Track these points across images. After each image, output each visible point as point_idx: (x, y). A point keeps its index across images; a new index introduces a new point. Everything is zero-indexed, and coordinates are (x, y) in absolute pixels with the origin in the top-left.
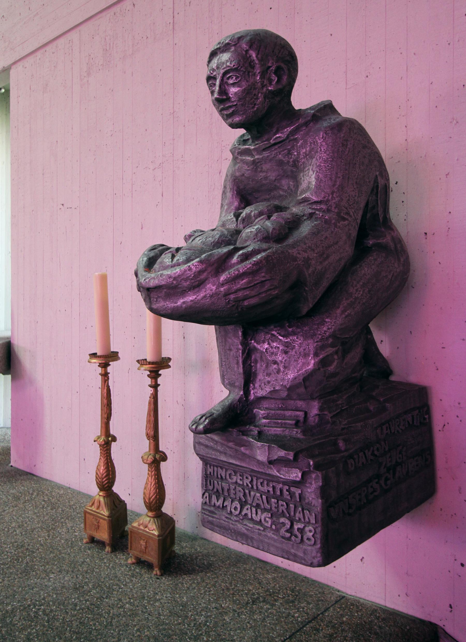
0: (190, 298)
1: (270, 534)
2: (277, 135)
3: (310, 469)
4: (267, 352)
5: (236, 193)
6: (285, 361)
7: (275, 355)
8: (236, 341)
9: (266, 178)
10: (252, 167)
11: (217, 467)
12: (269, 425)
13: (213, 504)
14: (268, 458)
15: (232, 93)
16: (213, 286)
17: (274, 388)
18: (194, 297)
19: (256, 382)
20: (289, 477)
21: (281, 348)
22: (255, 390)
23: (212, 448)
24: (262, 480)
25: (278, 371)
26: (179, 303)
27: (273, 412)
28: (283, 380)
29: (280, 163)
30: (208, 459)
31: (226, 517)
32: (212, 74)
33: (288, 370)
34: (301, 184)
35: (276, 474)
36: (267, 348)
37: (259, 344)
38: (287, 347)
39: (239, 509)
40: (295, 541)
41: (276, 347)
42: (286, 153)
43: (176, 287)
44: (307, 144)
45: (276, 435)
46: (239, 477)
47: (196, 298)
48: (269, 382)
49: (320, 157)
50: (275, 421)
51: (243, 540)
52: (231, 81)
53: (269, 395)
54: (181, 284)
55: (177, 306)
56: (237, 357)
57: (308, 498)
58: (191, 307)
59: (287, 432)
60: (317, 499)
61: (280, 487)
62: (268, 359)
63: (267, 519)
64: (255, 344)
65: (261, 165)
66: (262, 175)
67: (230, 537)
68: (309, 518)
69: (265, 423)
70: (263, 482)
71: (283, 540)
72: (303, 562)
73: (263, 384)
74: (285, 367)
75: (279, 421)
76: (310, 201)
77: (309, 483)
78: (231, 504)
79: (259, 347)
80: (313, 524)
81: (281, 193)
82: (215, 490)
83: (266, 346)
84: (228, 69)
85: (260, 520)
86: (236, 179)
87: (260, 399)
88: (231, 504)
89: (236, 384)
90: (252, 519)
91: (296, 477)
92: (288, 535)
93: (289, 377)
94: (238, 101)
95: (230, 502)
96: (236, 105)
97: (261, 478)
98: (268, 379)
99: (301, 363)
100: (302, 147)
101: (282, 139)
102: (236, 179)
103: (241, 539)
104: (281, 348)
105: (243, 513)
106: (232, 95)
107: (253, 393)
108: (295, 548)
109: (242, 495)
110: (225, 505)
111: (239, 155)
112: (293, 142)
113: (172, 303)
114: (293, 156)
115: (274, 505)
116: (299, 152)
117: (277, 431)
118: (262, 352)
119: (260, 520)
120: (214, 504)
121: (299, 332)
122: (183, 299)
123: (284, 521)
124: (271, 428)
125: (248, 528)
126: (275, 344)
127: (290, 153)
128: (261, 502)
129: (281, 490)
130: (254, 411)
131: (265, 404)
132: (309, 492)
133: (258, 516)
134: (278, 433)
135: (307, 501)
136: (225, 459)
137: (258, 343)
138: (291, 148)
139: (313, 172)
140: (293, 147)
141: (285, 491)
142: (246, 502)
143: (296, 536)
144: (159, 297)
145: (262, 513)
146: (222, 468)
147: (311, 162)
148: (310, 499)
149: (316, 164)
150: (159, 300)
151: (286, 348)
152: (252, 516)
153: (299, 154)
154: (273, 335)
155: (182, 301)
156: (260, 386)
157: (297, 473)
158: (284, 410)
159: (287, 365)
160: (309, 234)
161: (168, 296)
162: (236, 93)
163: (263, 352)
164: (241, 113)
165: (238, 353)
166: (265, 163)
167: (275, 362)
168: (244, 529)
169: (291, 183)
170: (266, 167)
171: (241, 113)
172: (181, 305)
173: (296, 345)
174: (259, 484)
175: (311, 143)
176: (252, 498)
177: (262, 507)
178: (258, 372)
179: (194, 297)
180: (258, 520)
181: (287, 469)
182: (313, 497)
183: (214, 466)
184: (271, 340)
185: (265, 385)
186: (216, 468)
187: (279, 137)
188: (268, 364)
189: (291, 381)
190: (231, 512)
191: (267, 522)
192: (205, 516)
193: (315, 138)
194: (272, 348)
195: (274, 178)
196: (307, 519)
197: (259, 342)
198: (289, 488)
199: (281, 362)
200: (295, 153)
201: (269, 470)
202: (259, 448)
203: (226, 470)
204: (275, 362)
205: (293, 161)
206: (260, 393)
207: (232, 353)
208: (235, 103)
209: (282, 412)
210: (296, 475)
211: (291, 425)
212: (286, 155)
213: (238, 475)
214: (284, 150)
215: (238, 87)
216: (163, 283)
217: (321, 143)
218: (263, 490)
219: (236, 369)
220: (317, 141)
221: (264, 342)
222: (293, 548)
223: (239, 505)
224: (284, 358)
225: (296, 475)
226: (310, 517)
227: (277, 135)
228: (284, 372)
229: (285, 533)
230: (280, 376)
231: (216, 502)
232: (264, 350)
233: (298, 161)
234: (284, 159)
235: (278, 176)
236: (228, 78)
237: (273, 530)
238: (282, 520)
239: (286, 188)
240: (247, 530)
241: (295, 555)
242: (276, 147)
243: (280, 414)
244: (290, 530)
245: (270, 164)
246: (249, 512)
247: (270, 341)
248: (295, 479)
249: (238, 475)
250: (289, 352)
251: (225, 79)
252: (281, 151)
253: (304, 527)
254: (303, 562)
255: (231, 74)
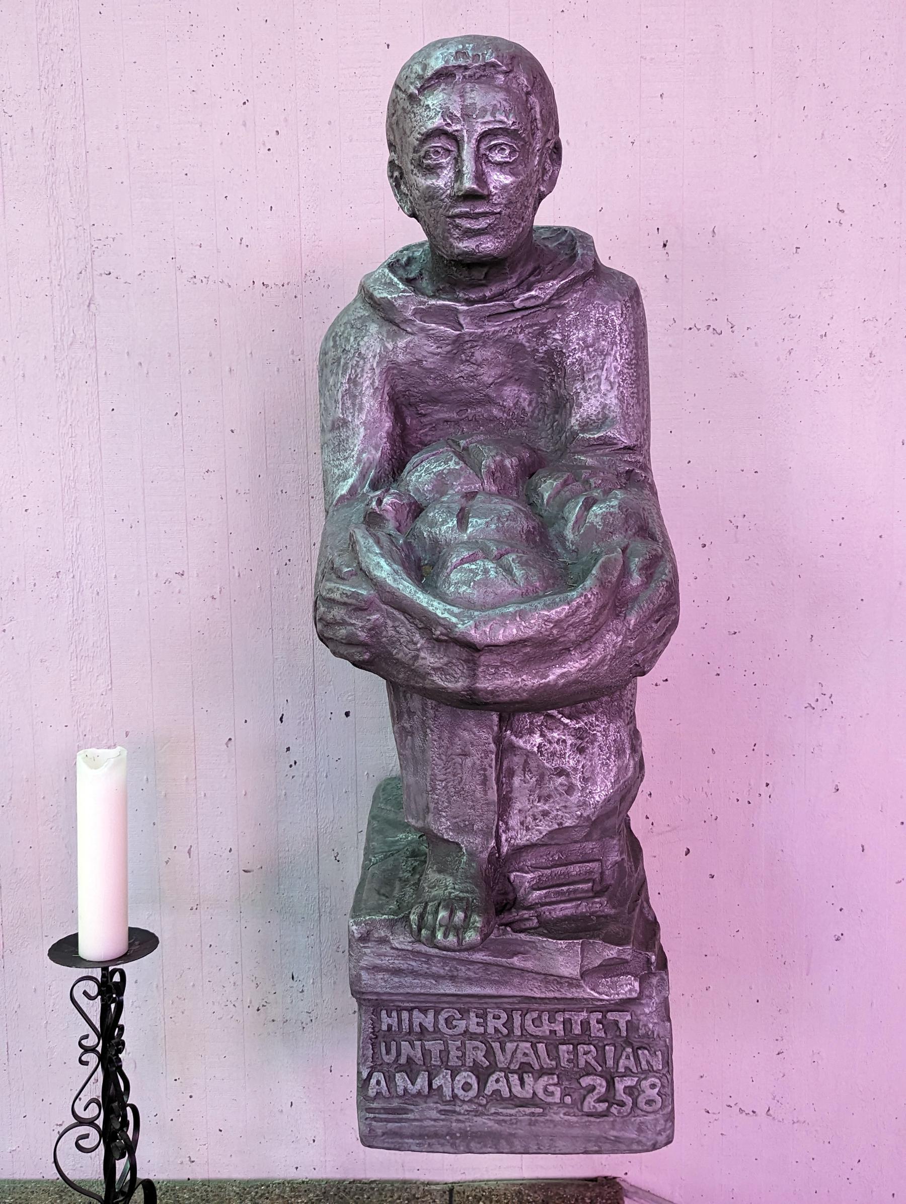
0: (574, 665)
1: (560, 1116)
2: (533, 293)
3: (649, 968)
4: (541, 752)
5: (387, 399)
6: (583, 767)
7: (560, 758)
8: (484, 735)
9: (473, 377)
10: (449, 348)
11: (410, 1010)
12: (548, 900)
13: (401, 1092)
14: (582, 967)
15: (497, 184)
16: (618, 635)
17: (560, 824)
18: (584, 662)
19: (509, 817)
20: (618, 994)
21: (569, 742)
22: (512, 833)
23: (414, 973)
24: (535, 1015)
25: (570, 789)
26: (552, 677)
27: (549, 871)
28: (583, 804)
29: (516, 350)
30: (384, 998)
31: (440, 1112)
32: (448, 125)
33: (592, 785)
34: (580, 406)
35: (590, 994)
36: (540, 744)
37: (521, 737)
38: (581, 738)
39: (475, 1086)
40: (619, 1112)
41: (559, 740)
42: (537, 332)
43: (554, 642)
44: (589, 321)
45: (566, 918)
46: (475, 1020)
47: (588, 664)
48: (545, 814)
49: (621, 355)
50: (557, 889)
51: (485, 1146)
52: (498, 157)
53: (546, 840)
54: (565, 636)
55: (547, 685)
56: (485, 770)
57: (645, 1025)
58: (576, 682)
59: (583, 908)
60: (662, 1023)
61: (582, 1018)
62: (544, 767)
63: (551, 1088)
64: (513, 738)
65: (472, 347)
66: (468, 369)
67: (451, 1150)
68: (648, 1062)
69: (540, 897)
70: (540, 1017)
71: (592, 1119)
72: (635, 1147)
73: (529, 819)
74: (585, 780)
75: (565, 888)
76: (616, 444)
77: (647, 996)
78: (453, 1080)
79: (521, 743)
80: (658, 1071)
81: (495, 412)
82: (403, 1060)
83: (537, 739)
84: (498, 126)
85: (534, 1093)
86: (393, 368)
87: (519, 851)
88: (453, 1080)
89: (475, 827)
90: (512, 1097)
91: (630, 990)
92: (603, 1106)
93: (597, 798)
94: (505, 205)
95: (449, 1076)
96: (500, 213)
97: (535, 1010)
98: (542, 806)
99: (615, 769)
100: (575, 323)
101: (540, 301)
102: (393, 368)
103: (479, 1146)
104: (569, 742)
105: (488, 1091)
106: (495, 188)
107: (506, 840)
108: (618, 1126)
109: (480, 1055)
110: (435, 1087)
111: (418, 316)
112: (555, 311)
113: (534, 678)
114: (549, 341)
115: (566, 1055)
116: (569, 336)
117: (567, 908)
118: (528, 754)
119: (534, 1093)
120: (405, 1090)
121: (596, 708)
122: (560, 667)
123: (592, 1083)
124: (555, 906)
125: (502, 1118)
126: (555, 735)
127: (542, 333)
128: (532, 1059)
129: (585, 1024)
130: (512, 877)
131: (529, 860)
132: (646, 1015)
133: (527, 1087)
134: (568, 912)
135: (642, 1032)
136: (453, 990)
137: (519, 735)
138: (549, 323)
139: (612, 384)
140: (553, 323)
141: (593, 1022)
142: (493, 1068)
143: (622, 1104)
144: (504, 664)
145: (536, 1080)
146: (424, 1011)
147: (604, 364)
148: (651, 1026)
149: (616, 368)
150: (502, 670)
151: (580, 742)
152: (510, 1091)
153: (565, 339)
154: (552, 717)
155: (558, 671)
156: (522, 823)
157: (630, 984)
158: (566, 865)
159: (587, 775)
160: (357, 481)
161: (528, 662)
162: (504, 188)
163: (533, 753)
164: (502, 233)
165: (486, 761)
166: (484, 346)
167: (561, 772)
168: (490, 1123)
169: (524, 395)
170: (480, 354)
171: (502, 233)
172: (556, 680)
173: (599, 734)
174: (442, 1022)
175: (598, 322)
176: (509, 1056)
177: (537, 1067)
178: (515, 794)
179: (584, 662)
180: (530, 1096)
181: (609, 980)
182: (656, 1021)
183: (399, 1010)
184: (546, 726)
185: (535, 819)
186: (405, 1015)
187: (532, 297)
188: (542, 776)
189: (601, 807)
190: (455, 1097)
191: (552, 1094)
192: (374, 1123)
193: (608, 314)
194: (550, 742)
195: (491, 380)
196: (644, 1066)
197: (520, 732)
198: (604, 1017)
199: (575, 769)
200: (557, 337)
201: (574, 990)
202: (560, 951)
203: (437, 1013)
204: (561, 772)
205: (546, 352)
206: (523, 838)
207: (469, 762)
208: (499, 210)
209: (563, 869)
210: (629, 987)
211: (587, 891)
212: (533, 337)
213: (472, 1014)
214: (531, 326)
215: (513, 174)
216: (530, 633)
217: (620, 325)
218: (540, 1034)
219: (478, 795)
220: (613, 321)
221: (531, 732)
222: (613, 1129)
223: (474, 1077)
224: (578, 761)
225: (629, 987)
226: (649, 1058)
227: (533, 293)
228: (583, 789)
229: (597, 1105)
230: (575, 798)
231: (410, 1086)
232: (535, 749)
233: (561, 354)
234: (527, 344)
235: (501, 376)
236: (491, 149)
237: (566, 1105)
238: (586, 1081)
239: (510, 403)
240: (499, 1122)
241: (617, 1140)
242: (518, 315)
243: (561, 875)
244: (609, 1098)
245: (493, 350)
246: (503, 1086)
247: (544, 729)
248: (628, 996)
249: (472, 1014)
250: (588, 748)
251: (483, 146)
252: (527, 327)
253: (639, 1082)
254: (635, 1147)
255: (500, 141)
